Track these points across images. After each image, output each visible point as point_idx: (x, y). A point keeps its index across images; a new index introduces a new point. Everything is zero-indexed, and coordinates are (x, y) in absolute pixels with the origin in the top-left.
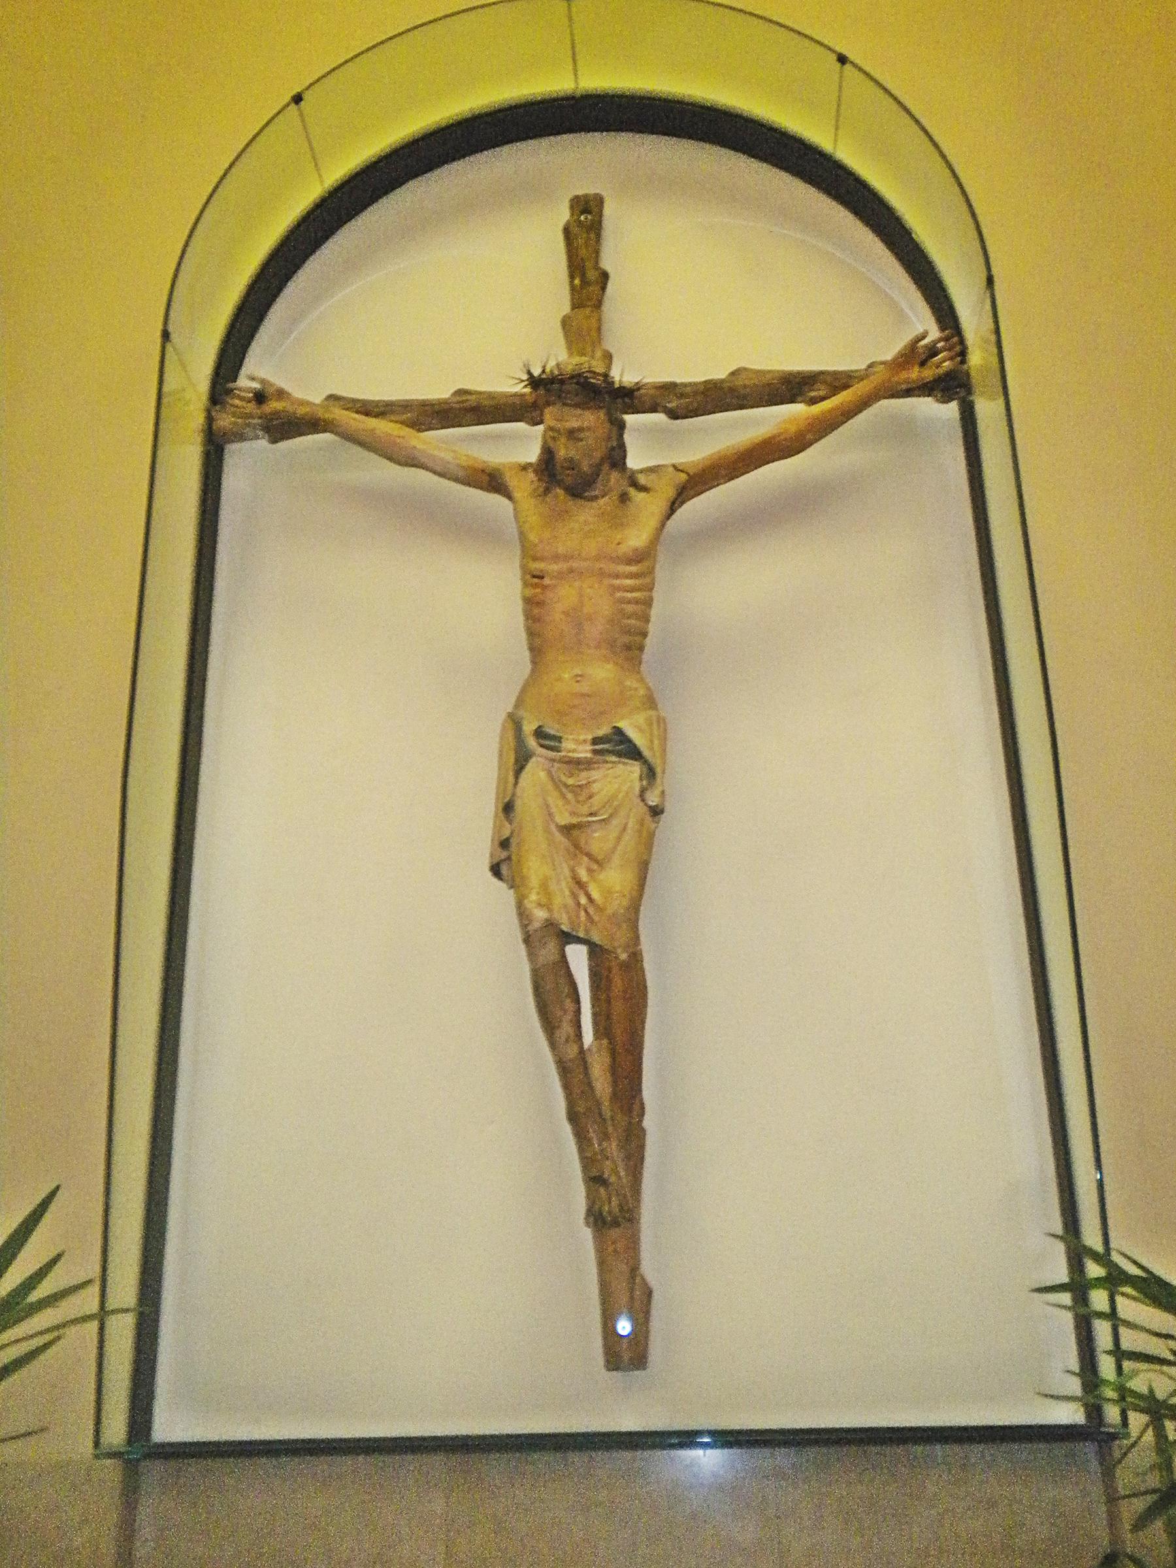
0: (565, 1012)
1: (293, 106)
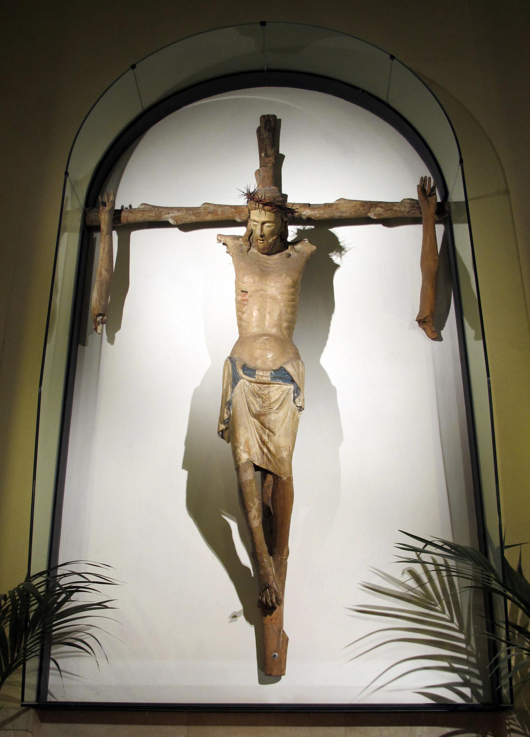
0: (254, 504)
1: (131, 70)
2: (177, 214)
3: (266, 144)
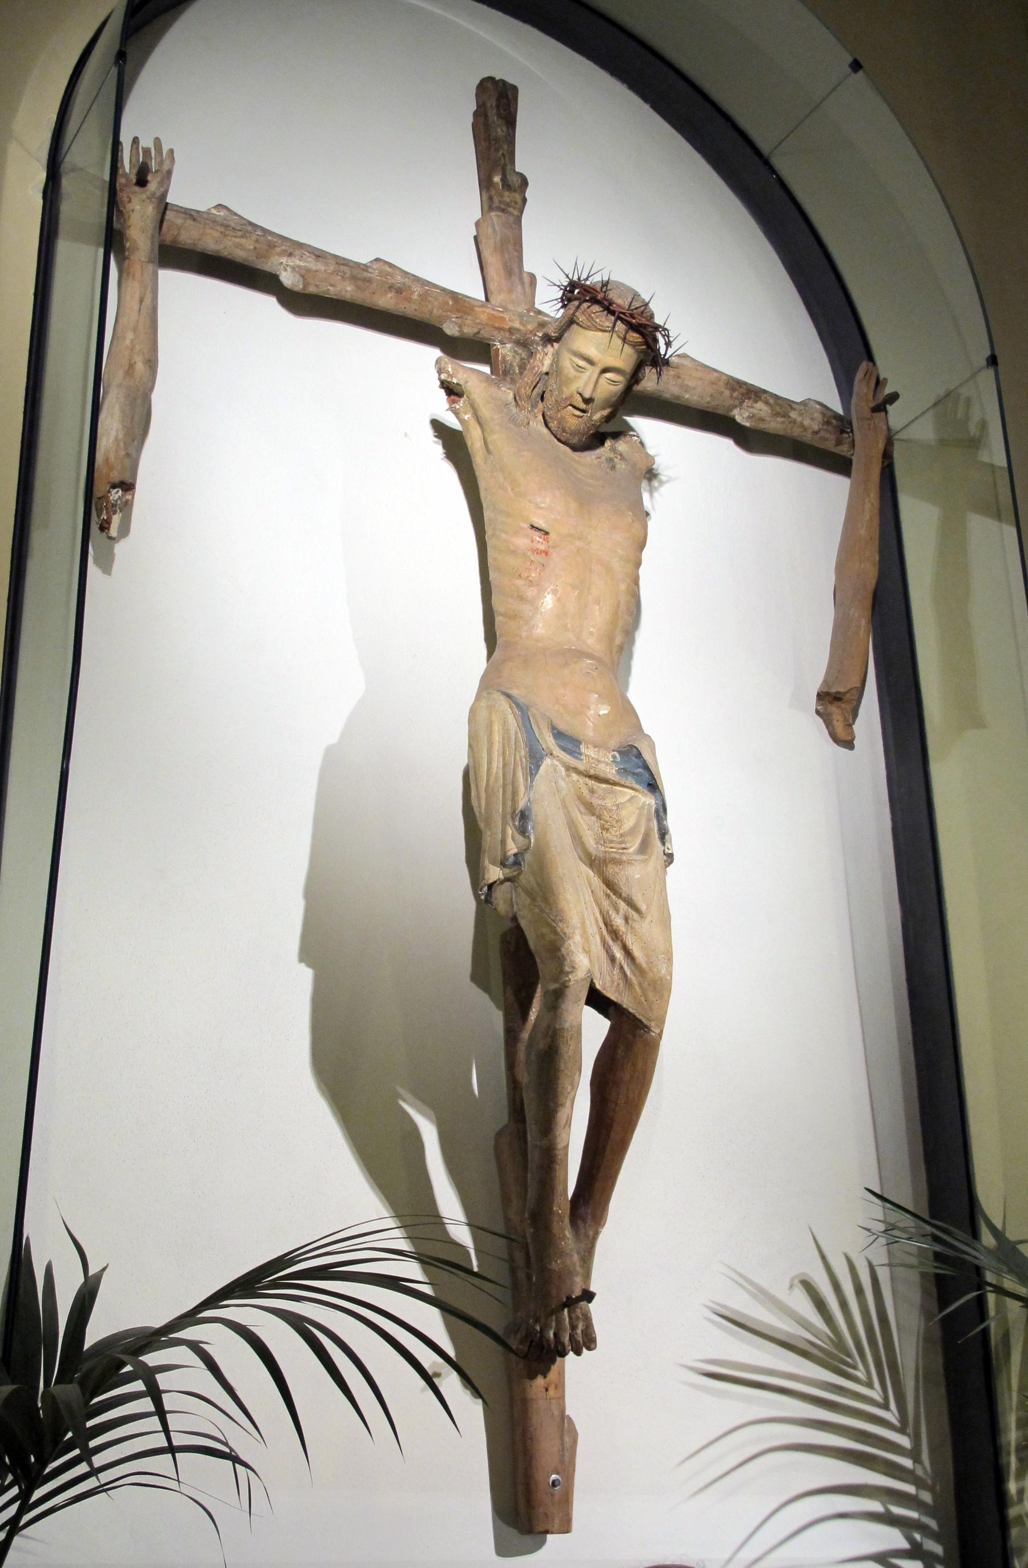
2: (312, 264)
3: (503, 155)
